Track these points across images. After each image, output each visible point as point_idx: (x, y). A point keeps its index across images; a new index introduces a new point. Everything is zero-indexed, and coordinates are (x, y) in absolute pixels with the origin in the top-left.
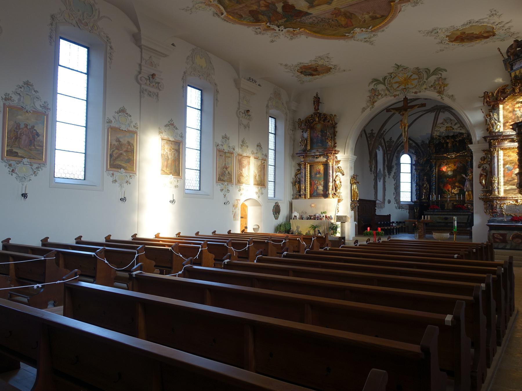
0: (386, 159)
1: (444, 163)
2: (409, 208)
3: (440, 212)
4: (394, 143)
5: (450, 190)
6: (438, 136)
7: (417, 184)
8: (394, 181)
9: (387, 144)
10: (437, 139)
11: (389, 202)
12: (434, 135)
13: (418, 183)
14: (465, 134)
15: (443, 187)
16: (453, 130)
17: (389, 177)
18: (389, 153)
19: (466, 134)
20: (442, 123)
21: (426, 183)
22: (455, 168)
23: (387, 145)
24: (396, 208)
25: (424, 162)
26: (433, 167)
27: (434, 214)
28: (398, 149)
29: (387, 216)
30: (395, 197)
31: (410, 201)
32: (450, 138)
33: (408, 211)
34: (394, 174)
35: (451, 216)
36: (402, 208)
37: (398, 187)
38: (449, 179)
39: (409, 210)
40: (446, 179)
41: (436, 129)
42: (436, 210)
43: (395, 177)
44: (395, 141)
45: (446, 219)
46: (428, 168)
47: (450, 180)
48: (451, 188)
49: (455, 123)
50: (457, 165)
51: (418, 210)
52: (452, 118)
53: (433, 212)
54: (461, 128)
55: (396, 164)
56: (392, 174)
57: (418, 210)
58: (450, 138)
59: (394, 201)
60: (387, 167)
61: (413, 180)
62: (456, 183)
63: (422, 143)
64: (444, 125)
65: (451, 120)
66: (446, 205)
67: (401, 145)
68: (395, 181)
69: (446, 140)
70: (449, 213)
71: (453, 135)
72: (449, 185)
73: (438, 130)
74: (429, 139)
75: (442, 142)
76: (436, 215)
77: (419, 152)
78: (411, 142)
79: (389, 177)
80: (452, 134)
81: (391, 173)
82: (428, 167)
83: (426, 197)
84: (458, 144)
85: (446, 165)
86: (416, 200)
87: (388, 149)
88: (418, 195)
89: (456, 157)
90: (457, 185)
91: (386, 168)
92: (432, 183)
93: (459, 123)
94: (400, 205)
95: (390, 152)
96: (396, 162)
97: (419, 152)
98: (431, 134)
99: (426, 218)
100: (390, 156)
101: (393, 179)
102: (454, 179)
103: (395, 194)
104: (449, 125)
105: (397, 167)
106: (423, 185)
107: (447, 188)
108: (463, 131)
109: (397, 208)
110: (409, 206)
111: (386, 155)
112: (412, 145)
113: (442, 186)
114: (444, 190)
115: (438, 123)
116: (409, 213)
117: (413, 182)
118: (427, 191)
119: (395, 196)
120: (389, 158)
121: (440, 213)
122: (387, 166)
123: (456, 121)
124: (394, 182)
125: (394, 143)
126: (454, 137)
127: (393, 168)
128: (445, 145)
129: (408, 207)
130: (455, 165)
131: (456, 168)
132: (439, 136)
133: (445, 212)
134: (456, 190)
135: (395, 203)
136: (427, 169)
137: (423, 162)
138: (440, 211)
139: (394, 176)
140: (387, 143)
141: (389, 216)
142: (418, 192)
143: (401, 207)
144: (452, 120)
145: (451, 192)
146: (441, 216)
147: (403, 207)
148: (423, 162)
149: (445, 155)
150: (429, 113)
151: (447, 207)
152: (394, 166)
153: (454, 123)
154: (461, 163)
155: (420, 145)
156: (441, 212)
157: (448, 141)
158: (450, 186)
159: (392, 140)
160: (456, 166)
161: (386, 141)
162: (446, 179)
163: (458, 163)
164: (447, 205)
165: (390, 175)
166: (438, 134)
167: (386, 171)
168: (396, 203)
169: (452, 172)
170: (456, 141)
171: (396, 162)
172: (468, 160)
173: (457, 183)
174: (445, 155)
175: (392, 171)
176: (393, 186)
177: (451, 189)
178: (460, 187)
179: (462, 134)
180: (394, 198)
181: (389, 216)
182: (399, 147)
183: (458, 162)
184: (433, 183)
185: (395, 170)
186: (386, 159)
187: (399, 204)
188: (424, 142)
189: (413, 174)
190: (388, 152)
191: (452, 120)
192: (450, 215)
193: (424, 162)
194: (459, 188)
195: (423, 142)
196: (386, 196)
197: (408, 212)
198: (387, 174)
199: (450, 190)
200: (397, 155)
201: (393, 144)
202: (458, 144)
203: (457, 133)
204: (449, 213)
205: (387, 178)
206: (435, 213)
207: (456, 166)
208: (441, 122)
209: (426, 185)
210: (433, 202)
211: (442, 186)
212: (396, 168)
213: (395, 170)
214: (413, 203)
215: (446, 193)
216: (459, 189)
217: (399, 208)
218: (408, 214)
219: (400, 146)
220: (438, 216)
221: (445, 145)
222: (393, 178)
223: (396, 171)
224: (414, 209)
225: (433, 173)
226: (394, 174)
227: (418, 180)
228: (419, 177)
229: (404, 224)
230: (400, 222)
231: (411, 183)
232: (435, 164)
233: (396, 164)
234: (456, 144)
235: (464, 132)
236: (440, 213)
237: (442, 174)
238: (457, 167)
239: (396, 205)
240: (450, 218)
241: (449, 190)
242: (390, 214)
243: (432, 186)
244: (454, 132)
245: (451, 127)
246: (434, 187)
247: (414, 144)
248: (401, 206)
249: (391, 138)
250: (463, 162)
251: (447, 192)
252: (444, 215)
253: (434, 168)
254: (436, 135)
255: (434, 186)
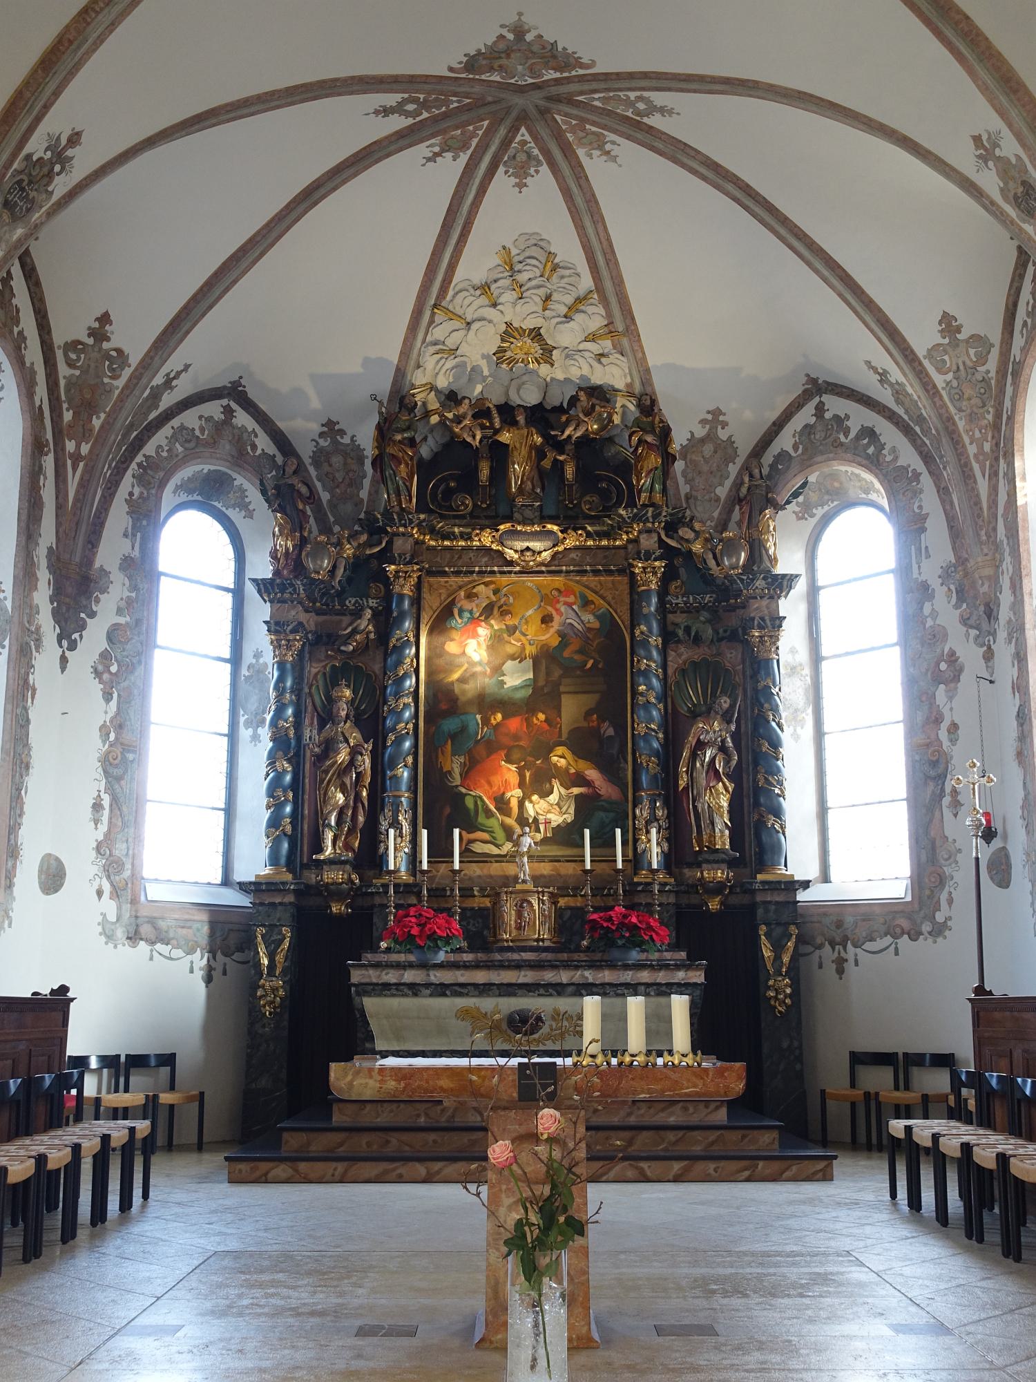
0: (48, 494)
1: (470, 596)
2: (212, 934)
3: (466, 966)
4: (127, 373)
5: (514, 804)
6: (438, 392)
7: (279, 740)
8: (108, 697)
9: (63, 370)
10: (434, 419)
11: (53, 878)
12: (419, 378)
13: (292, 733)
14: (620, 401)
15: (465, 775)
16: (544, 370)
17: (64, 660)
18: (76, 458)
19: (631, 394)
20: (485, 288)
21: (355, 737)
22: (550, 637)
23: (62, 383)
24: (109, 937)
25: (340, 572)
26: (402, 616)
27: (427, 985)
28: (149, 449)
29: (35, 1004)
30: (108, 835)
31: (217, 877)
32: (521, 419)
33: (200, 960)
34: (110, 638)
35: (563, 1004)
36: (160, 937)
37: (130, 756)
38: (504, 718)
39: (212, 952)
40: (486, 721)
41: (438, 333)
42: (441, 956)
43: (114, 669)
44: (134, 360)
45: (522, 1023)
46: (365, 623)
47: (515, 724)
48: (521, 785)
49: (569, 300)
50: (568, 615)
51: (280, 958)
52: (569, 249)
53: (424, 966)
54: (607, 344)
55: (128, 564)
56: (94, 638)
57: (280, 958)
58: (521, 419)
59: (95, 870)
60: (50, 567)
61: (242, 720)
62: (551, 750)
63: (323, 443)
64: (494, 305)
65: (553, 266)
66: (509, 913)
67: (175, 422)
68: (113, 704)
69: (497, 432)
70: (549, 976)
71: (540, 407)
72: (509, 761)
73: (451, 343)
74: (381, 402)
75: (469, 440)
76: (442, 990)
77: (304, 490)
78: (243, 419)
79: (64, 660)
80: (531, 397)
81: (82, 627)
82: (368, 614)
83: (347, 847)
84: (570, 471)
85: (488, 611)
86: (267, 871)
87: (68, 416)
88: (289, 829)
89: (553, 567)
90: (562, 762)
91: (44, 576)
92: (392, 737)
93: (604, 301)
94: (144, 912)
95: (85, 449)
96: (125, 547)
97: (304, 490)
98: (400, 373)
99: (636, 1039)
100: (84, 485)
101: (97, 688)
102: (542, 716)
103: (106, 813)
104: (525, 315)
105: (134, 588)
106: (328, 748)
107: (489, 783)
108: (615, 374)
109: (120, 933)
110: (213, 925)
111: (49, 462)
112: (254, 447)
113: (457, 771)
114: (469, 802)
115: (460, 274)
116: (209, 979)
117: (245, 733)
118: (358, 797)
119: (103, 828)
120: (76, 500)
121: (526, 977)
122: (57, 562)
123: (587, 282)
124: (103, 712)
125: (127, 373)
126: (541, 416)
127: (104, 591)
128: (484, 472)
129: (206, 929)
130: (546, 620)
131: (555, 642)
132: (452, 398)
133: (502, 966)
134: (554, 798)
135: (100, 893)
136: (355, 631)
137: (334, 567)
138: (468, 957)
139: (105, 656)
140: (71, 364)
141: (59, 1001)
142: (288, 809)
143: (146, 929)
144: (555, 267)
145: (522, 821)
146: (487, 1004)
147: (163, 924)
148: (334, 567)
149: (486, 539)
150: (423, 150)
151: (519, 927)
152: (107, 573)
153: (563, 300)
154: (586, 603)
155: (306, 451)
156: (477, 966)
157: (505, 437)
158: (509, 773)
159: (105, 345)
160: (556, 625)
161: (59, 338)
162: (486, 721)
163: (570, 605)
164: (519, 915)
165: (73, 646)
166: (442, 383)
167: (42, 596)
168: (107, 887)
169: (525, 671)
170: (559, 446)
171: (125, 547)
172: (647, 583)
173: (560, 750)
174: (486, 539)
175: (92, 615)
176: (95, 747)
177: (518, 792)
178: (580, 780)
179: (599, 394)
180: (98, 849)
181: (59, 1001)
182: (161, 437)
183: (571, 599)
184: (399, 740)
185: (119, 612)
186: (48, 494)
187: (134, 901)
188: (342, 432)
189: (244, 672)
190: (70, 446)
191: (555, 267)
192: (558, 989)
193: (340, 572)
194: (576, 791)
195: (331, 428)
196: (25, 820)
197: (199, 975)
198: (46, 621)
199: (514, 804)
200: (137, 491)
201: (120, 383)
202: (570, 471)
203: (570, 392)
204: (549, 976)
205: (50, 651)
206: (437, 977)
207: (556, 625)
208: (479, 277)
209: (355, 752)
210: (405, 890)
211: (454, 765)
212: (127, 594)
213: (119, 612)
214: (243, 900)
215: (481, 819)
216: (578, 798)
217: (134, 937)
218: (202, 986)
219: (166, 431)
220: (461, 1002)
221: (484, 472)
222: (97, 673)
223: (122, 620)
224: (248, 943)
225: (400, 662)
226: (104, 645)
227: (290, 711)
228: (297, 690)
229: (165, 1070)
230: (137, 1061)
231: (232, 736)
232: (417, 601)
233: (128, 564)
234: (558, 466)
235: (620, 384)
236: (526, 977)
237: (456, 676)
238: (561, 634)
239: (109, 907)
240: (557, 1015)
241: (502, 804)
242: (64, 989)
243: (393, 765)
244: (546, 387)
245: (536, 334)
246: (406, 774)
247: (264, 443)
248: (152, 921)
249: (105, 319)
250: (603, 598)
251: (489, 814)
252: (508, 990)
253: (407, 624)
254: (432, 388)
255: (410, 759)
